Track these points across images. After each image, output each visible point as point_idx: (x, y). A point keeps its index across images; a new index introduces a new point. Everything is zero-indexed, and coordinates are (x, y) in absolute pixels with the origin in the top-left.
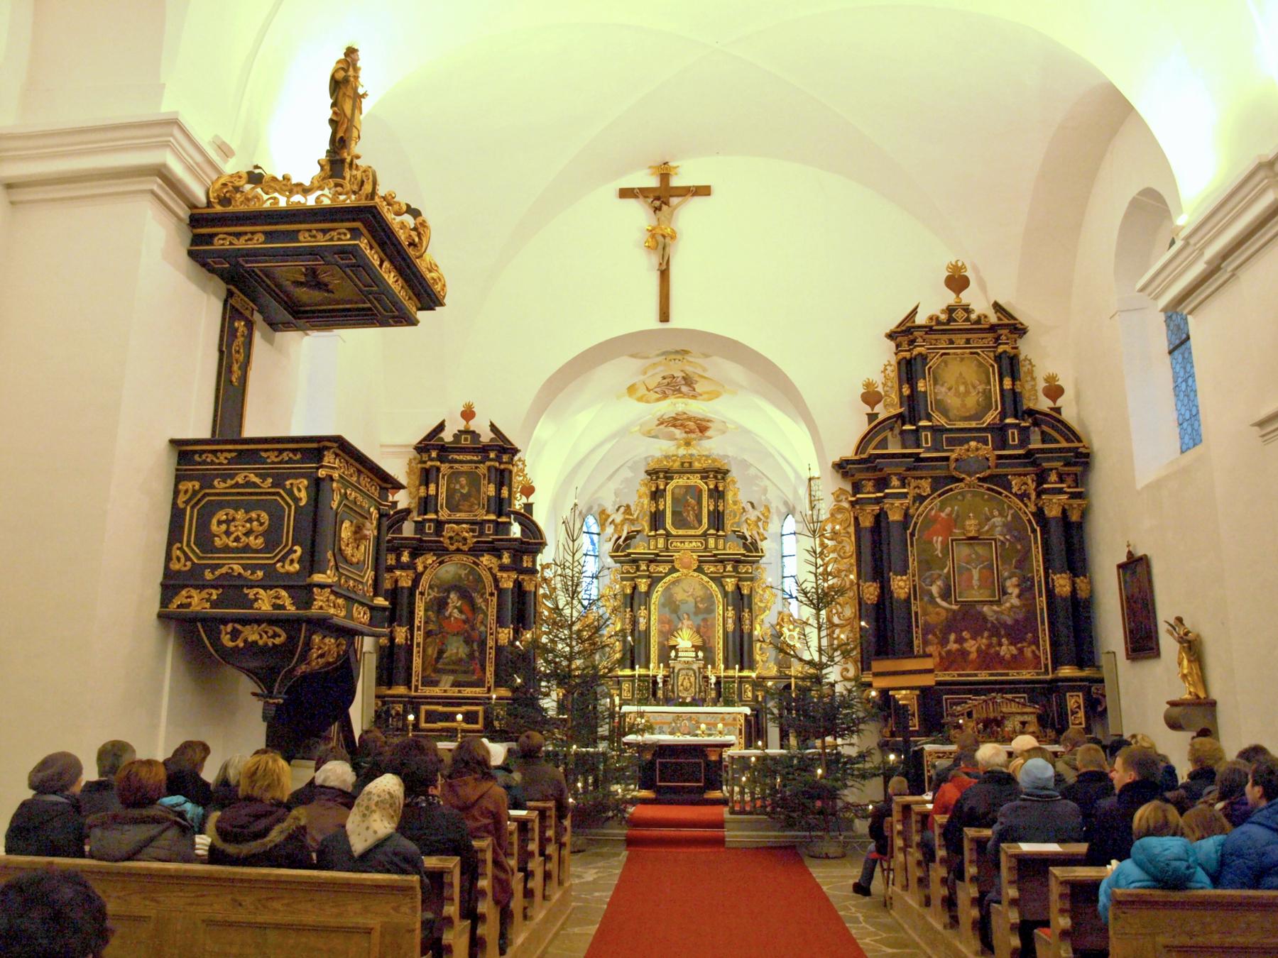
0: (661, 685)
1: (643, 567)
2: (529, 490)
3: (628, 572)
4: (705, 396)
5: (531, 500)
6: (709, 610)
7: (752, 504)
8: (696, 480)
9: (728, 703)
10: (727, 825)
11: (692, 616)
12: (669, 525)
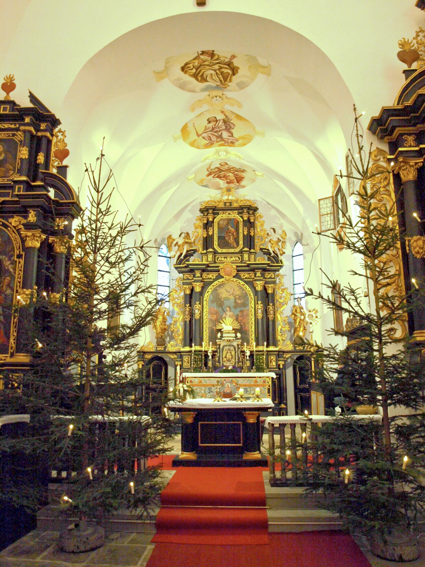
0: (210, 357)
1: (198, 274)
2: (64, 154)
3: (188, 279)
4: (240, 141)
5: (65, 162)
6: (245, 304)
7: (274, 230)
8: (234, 215)
9: (260, 369)
10: (268, 501)
11: (232, 309)
12: (216, 246)
